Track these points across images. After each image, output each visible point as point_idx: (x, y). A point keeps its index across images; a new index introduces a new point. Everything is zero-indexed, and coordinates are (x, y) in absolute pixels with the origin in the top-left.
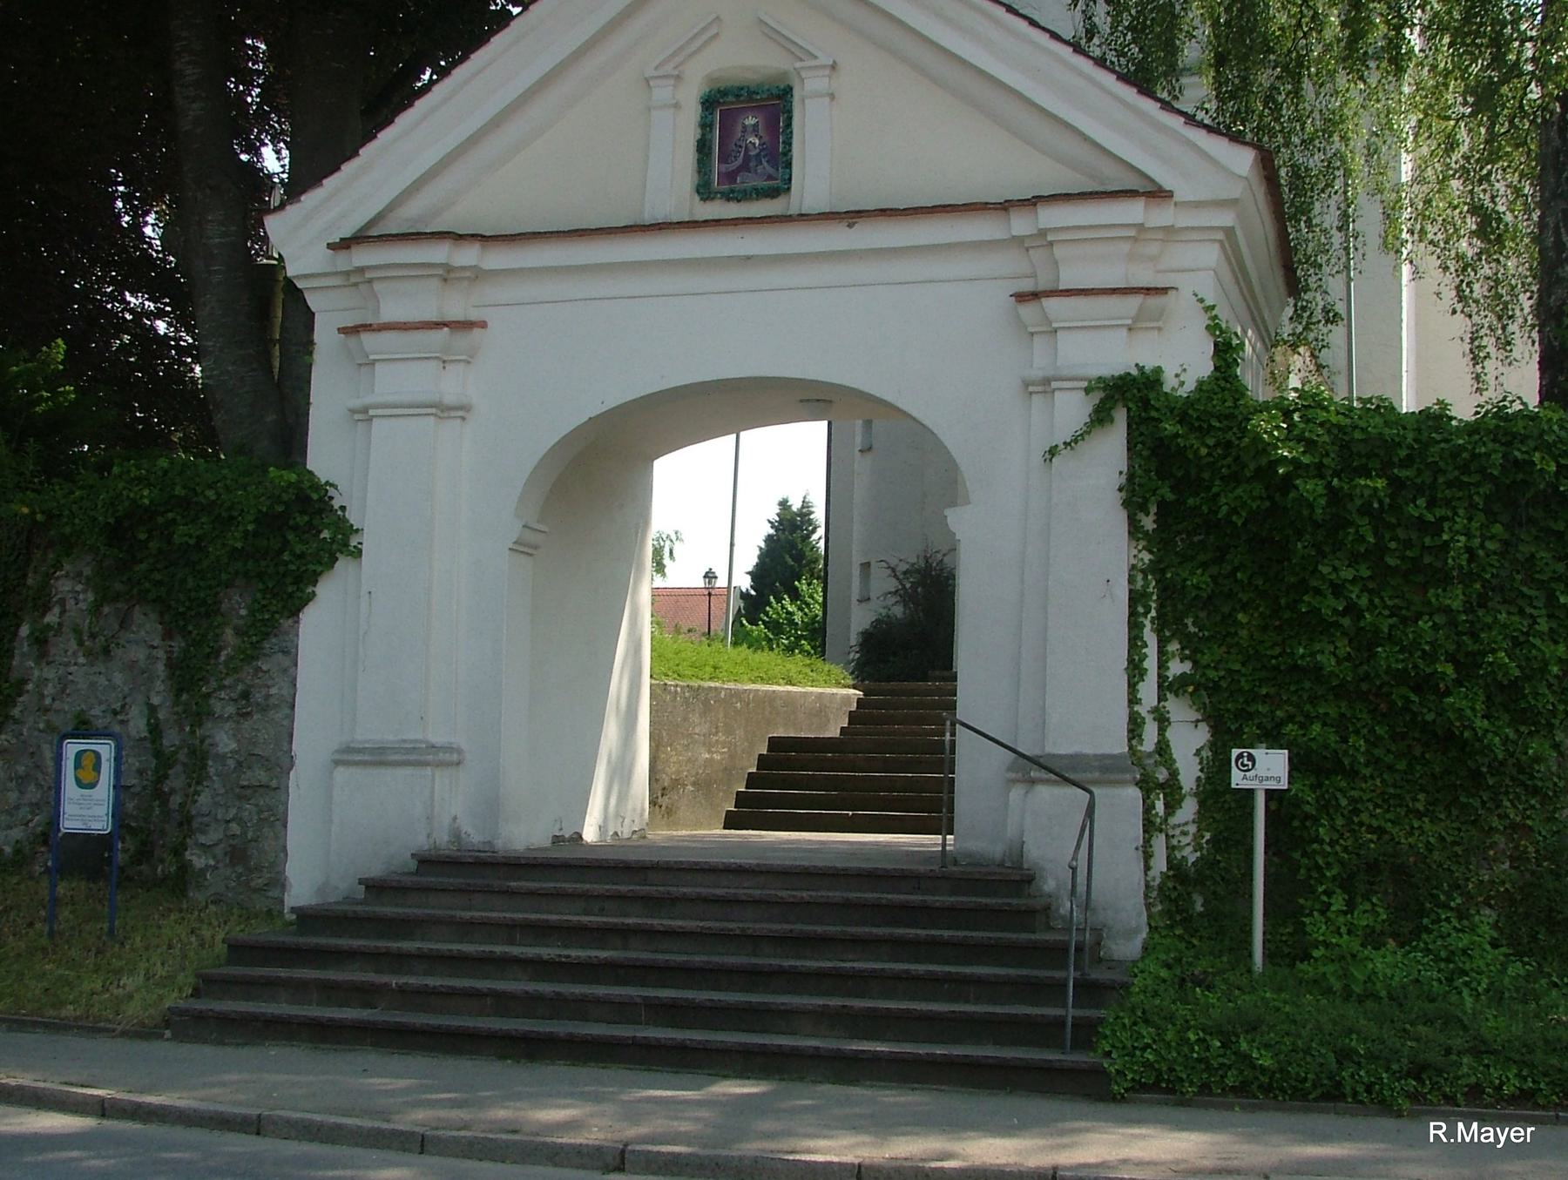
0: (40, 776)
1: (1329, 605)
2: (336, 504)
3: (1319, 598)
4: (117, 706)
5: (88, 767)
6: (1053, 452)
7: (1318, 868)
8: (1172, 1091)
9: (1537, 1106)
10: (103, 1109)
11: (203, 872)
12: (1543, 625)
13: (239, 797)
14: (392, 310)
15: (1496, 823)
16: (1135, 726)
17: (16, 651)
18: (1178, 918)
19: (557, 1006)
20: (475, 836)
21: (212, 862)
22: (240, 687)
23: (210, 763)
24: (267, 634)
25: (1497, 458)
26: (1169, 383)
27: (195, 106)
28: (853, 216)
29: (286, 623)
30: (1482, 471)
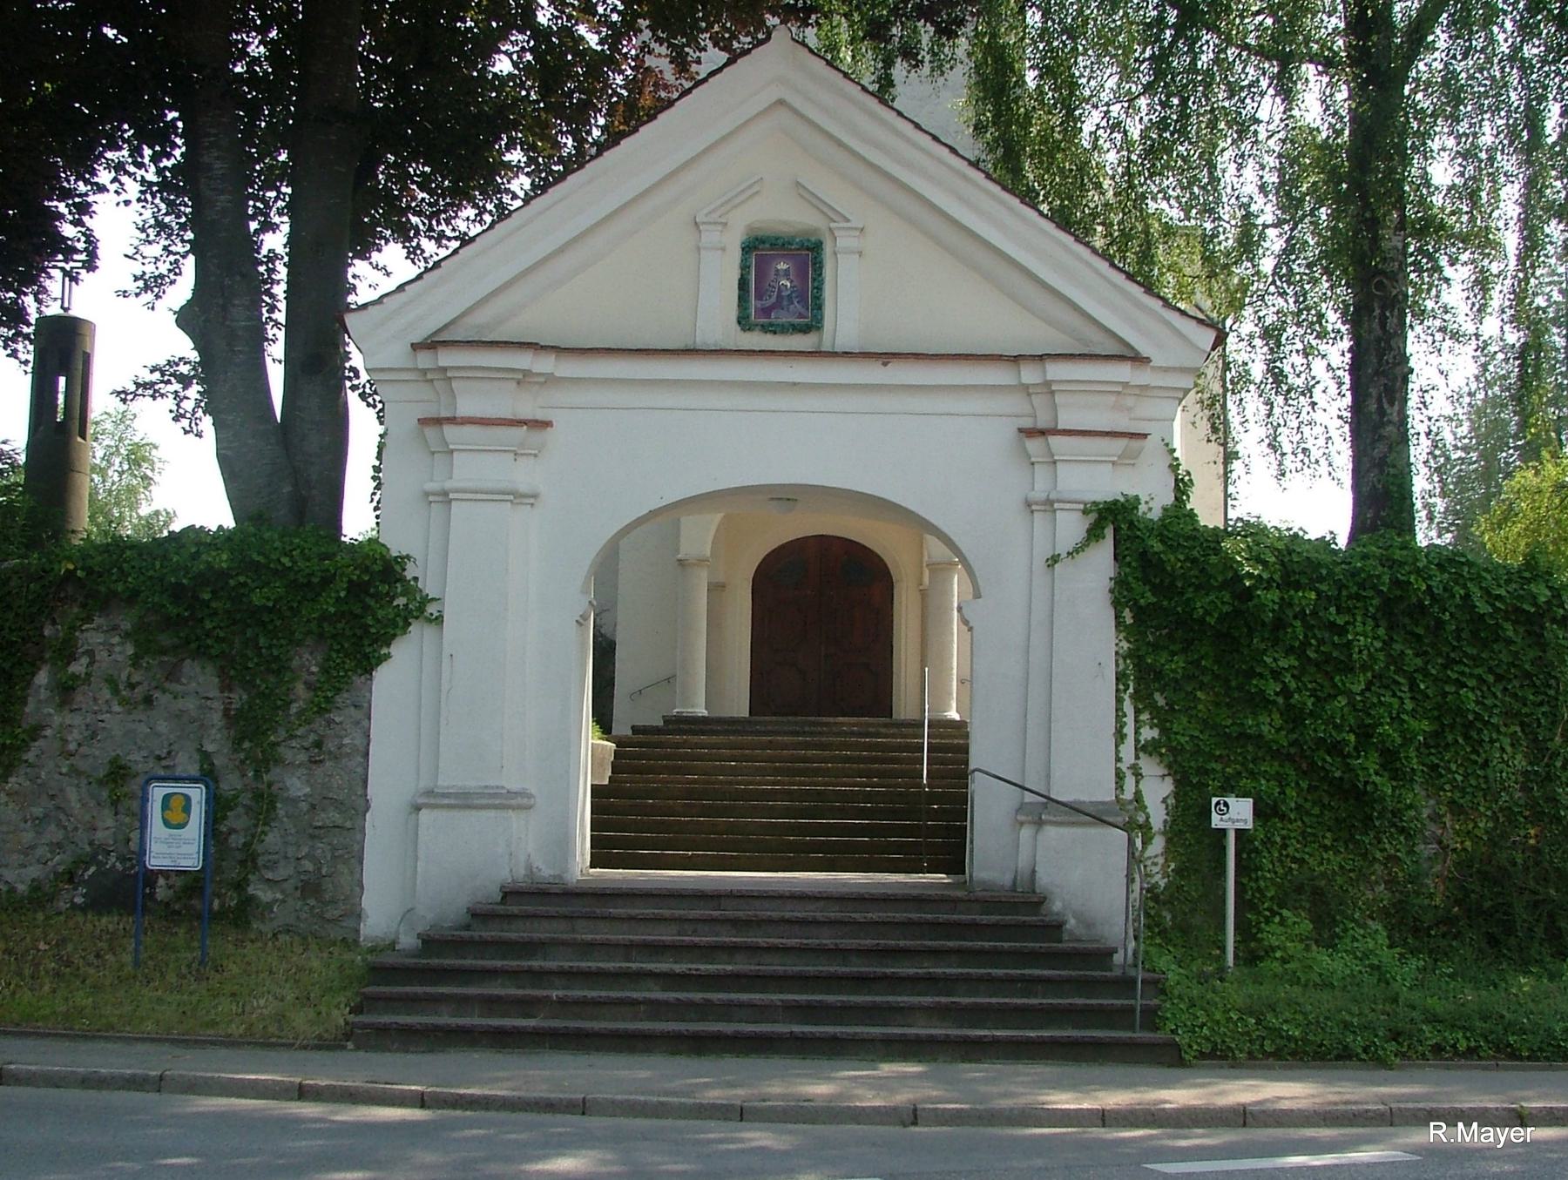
0: (62, 816)
1: (1272, 688)
2: (409, 575)
3: (1263, 682)
4: (163, 753)
5: (176, 812)
6: (1054, 560)
7: (1259, 889)
8: (1225, 1058)
9: (1480, 1058)
10: (421, 1101)
11: (269, 906)
12: (1409, 705)
13: (312, 837)
14: (465, 408)
15: (1378, 855)
16: (1120, 776)
17: (30, 699)
18: (1157, 930)
19: (704, 1010)
20: (546, 871)
21: (279, 896)
22: (312, 737)
23: (279, 805)
24: (340, 690)
25: (1386, 579)
26: (1142, 508)
27: (222, 197)
28: (887, 357)
29: (358, 680)
30: (1374, 587)
